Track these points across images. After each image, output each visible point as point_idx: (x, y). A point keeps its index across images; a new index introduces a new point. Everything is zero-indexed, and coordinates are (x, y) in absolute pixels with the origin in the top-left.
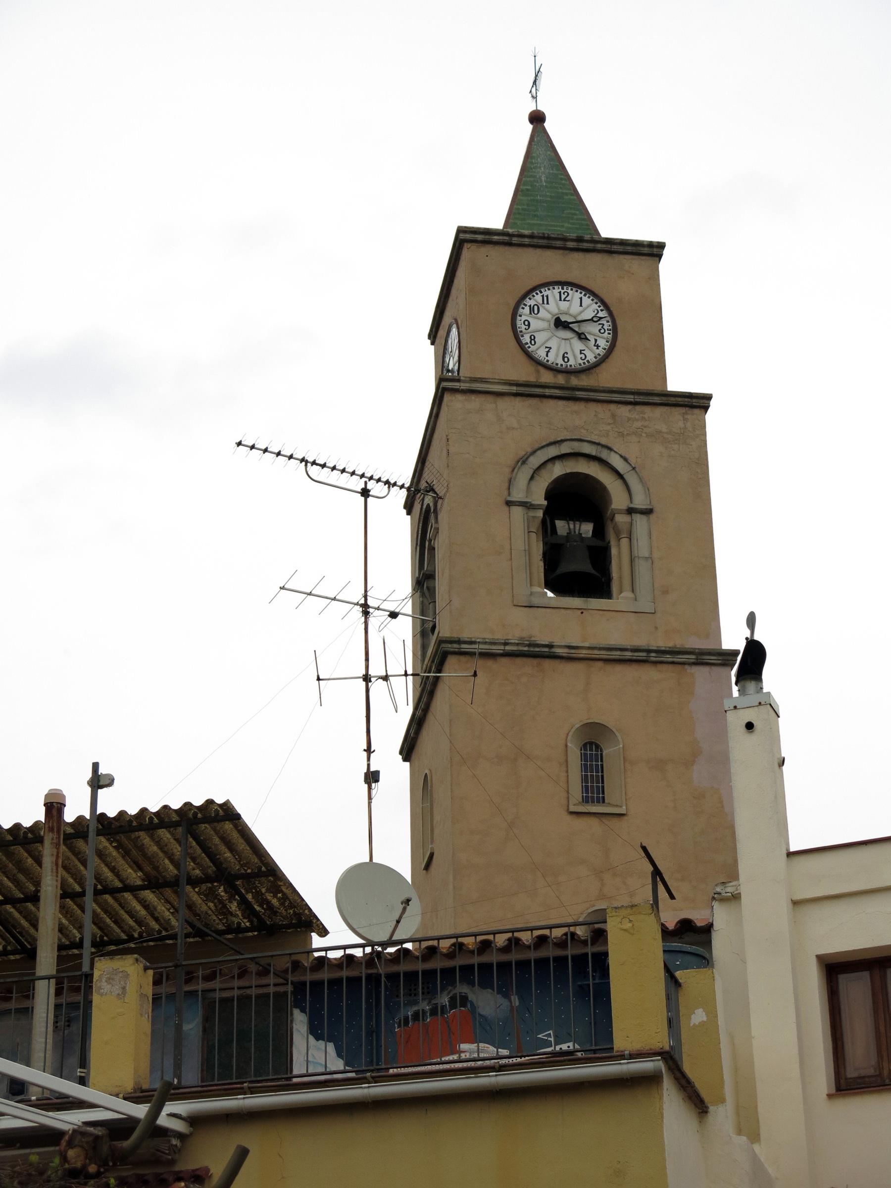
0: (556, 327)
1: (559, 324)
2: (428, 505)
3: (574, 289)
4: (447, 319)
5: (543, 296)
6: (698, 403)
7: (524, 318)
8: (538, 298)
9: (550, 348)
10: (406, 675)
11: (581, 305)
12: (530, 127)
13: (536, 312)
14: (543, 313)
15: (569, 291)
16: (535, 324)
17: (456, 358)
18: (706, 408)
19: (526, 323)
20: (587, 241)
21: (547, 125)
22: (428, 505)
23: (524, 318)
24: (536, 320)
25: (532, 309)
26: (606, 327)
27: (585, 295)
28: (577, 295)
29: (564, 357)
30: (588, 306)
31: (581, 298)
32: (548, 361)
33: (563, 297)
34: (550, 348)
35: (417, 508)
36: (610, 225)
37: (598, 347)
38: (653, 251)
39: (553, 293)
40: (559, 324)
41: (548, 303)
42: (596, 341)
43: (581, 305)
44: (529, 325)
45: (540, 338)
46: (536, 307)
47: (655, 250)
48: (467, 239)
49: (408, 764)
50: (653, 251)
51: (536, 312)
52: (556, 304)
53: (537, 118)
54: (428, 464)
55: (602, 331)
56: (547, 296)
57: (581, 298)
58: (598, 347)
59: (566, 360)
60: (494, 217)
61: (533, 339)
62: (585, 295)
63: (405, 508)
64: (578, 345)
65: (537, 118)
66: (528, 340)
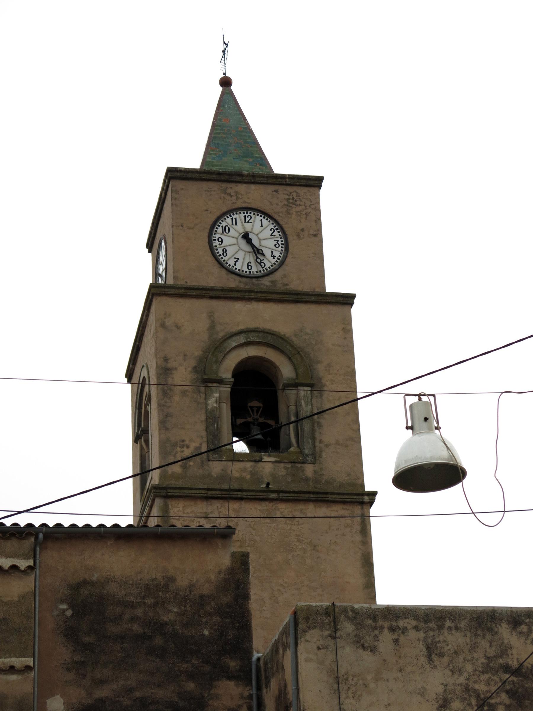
0: (246, 240)
1: (246, 236)
2: (144, 377)
3: (256, 213)
4: (159, 236)
5: (232, 219)
6: (348, 300)
7: (217, 236)
8: (229, 220)
9: (238, 259)
10: (139, 384)
11: (262, 226)
12: (220, 89)
13: (227, 231)
14: (232, 232)
15: (252, 215)
16: (227, 240)
17: (164, 266)
18: (351, 304)
19: (220, 240)
20: (264, 177)
21: (232, 87)
22: (144, 377)
23: (217, 236)
24: (227, 237)
25: (224, 229)
26: (280, 243)
27: (264, 217)
28: (258, 218)
29: (248, 266)
30: (266, 227)
31: (261, 220)
32: (236, 269)
33: (247, 219)
34: (238, 259)
35: (135, 379)
36: (280, 165)
37: (274, 257)
38: (315, 183)
39: (240, 217)
40: (246, 236)
41: (236, 224)
42: (272, 252)
43: (262, 226)
44: (222, 241)
45: (230, 251)
46: (227, 228)
47: (316, 183)
48: (174, 175)
49: (150, 254)
50: (315, 183)
51: (227, 231)
52: (239, 224)
53: (226, 82)
54: (141, 353)
55: (277, 246)
56: (236, 219)
57: (261, 220)
58: (274, 257)
59: (250, 267)
60: (193, 161)
61: (225, 251)
62: (264, 217)
63: (126, 377)
64: (250, 258)
65: (226, 82)
66: (221, 253)
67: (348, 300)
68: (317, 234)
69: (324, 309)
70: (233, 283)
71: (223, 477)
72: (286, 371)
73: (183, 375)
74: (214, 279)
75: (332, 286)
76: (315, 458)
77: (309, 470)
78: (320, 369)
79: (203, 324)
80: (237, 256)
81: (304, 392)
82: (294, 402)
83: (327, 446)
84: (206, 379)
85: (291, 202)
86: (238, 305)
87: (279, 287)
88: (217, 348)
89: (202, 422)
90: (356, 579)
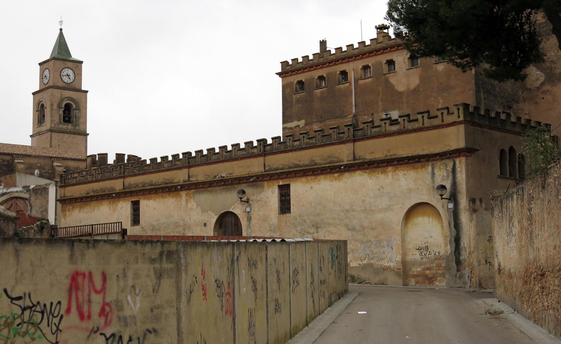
0: (68, 75)
6: (87, 92)
38: (81, 62)
39: (66, 69)
50: (81, 62)
53: (61, 30)
65: (61, 30)
67: (87, 92)
68: (81, 75)
69: (82, 93)
70: (64, 85)
71: (61, 128)
72: (74, 106)
73: (55, 106)
74: (61, 84)
75: (83, 89)
76: (78, 125)
77: (77, 128)
78: (81, 107)
79: (59, 95)
80: (66, 79)
81: (77, 111)
82: (74, 113)
83: (159, 276)
84: (59, 107)
85: (76, 67)
86: (66, 91)
87: (73, 87)
88: (62, 100)
89: (69, 137)
90: (84, 151)
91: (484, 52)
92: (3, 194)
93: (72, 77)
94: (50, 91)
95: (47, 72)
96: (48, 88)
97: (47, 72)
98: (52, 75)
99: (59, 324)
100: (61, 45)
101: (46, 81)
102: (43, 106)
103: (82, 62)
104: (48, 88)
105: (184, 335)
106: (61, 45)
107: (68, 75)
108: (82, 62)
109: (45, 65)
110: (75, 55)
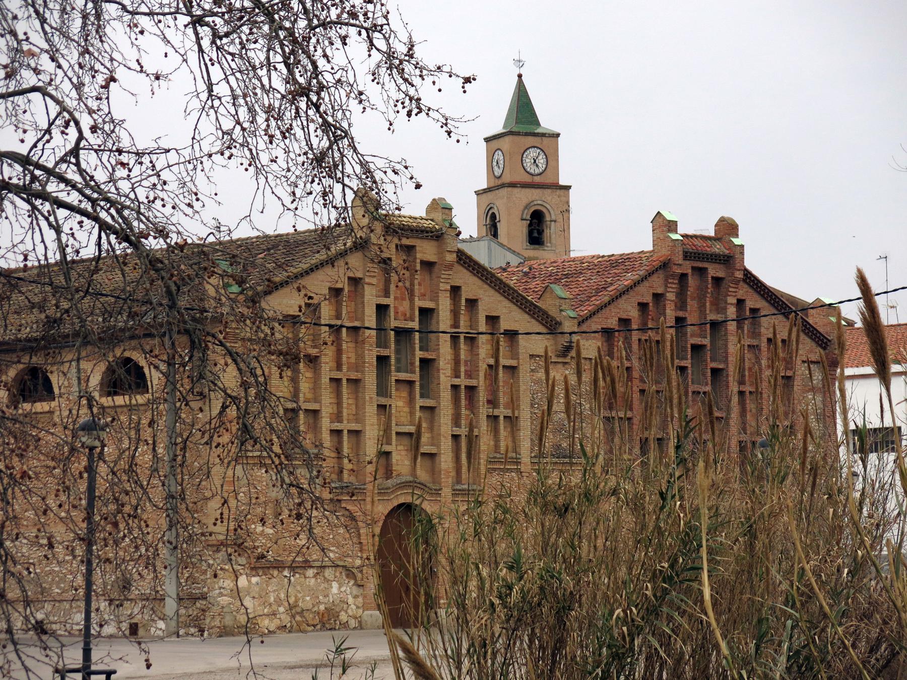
6: (568, 188)
53: (520, 76)
65: (520, 76)
68: (557, 160)
75: (562, 182)
91: (833, 316)
92: (399, 673)
93: (541, 161)
94: (504, 192)
95: (499, 156)
96: (503, 186)
97: (499, 156)
98: (507, 158)
99: (343, 190)
100: (522, 106)
101: (498, 172)
102: (493, 216)
103: (558, 135)
104: (503, 186)
105: (376, 433)
106: (522, 106)
107: (535, 161)
108: (558, 135)
109: (495, 144)
110: (547, 122)
